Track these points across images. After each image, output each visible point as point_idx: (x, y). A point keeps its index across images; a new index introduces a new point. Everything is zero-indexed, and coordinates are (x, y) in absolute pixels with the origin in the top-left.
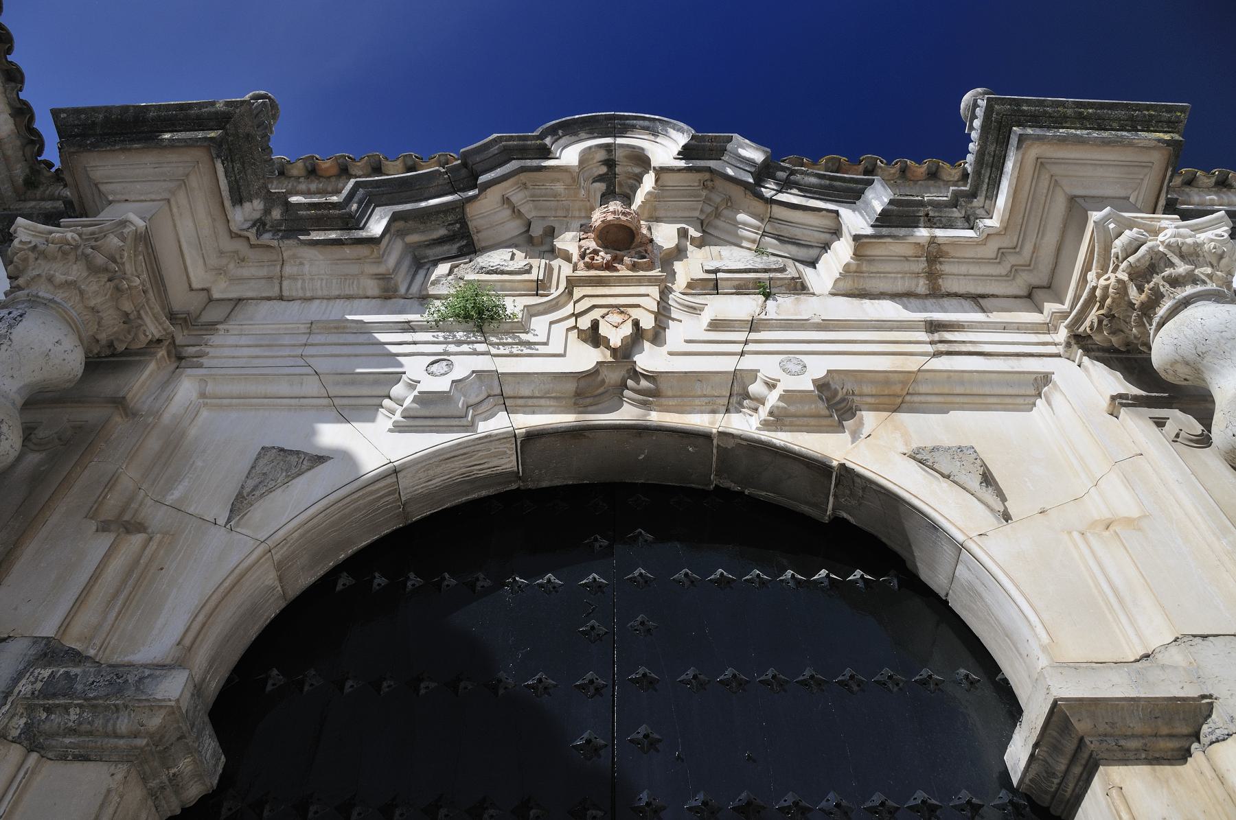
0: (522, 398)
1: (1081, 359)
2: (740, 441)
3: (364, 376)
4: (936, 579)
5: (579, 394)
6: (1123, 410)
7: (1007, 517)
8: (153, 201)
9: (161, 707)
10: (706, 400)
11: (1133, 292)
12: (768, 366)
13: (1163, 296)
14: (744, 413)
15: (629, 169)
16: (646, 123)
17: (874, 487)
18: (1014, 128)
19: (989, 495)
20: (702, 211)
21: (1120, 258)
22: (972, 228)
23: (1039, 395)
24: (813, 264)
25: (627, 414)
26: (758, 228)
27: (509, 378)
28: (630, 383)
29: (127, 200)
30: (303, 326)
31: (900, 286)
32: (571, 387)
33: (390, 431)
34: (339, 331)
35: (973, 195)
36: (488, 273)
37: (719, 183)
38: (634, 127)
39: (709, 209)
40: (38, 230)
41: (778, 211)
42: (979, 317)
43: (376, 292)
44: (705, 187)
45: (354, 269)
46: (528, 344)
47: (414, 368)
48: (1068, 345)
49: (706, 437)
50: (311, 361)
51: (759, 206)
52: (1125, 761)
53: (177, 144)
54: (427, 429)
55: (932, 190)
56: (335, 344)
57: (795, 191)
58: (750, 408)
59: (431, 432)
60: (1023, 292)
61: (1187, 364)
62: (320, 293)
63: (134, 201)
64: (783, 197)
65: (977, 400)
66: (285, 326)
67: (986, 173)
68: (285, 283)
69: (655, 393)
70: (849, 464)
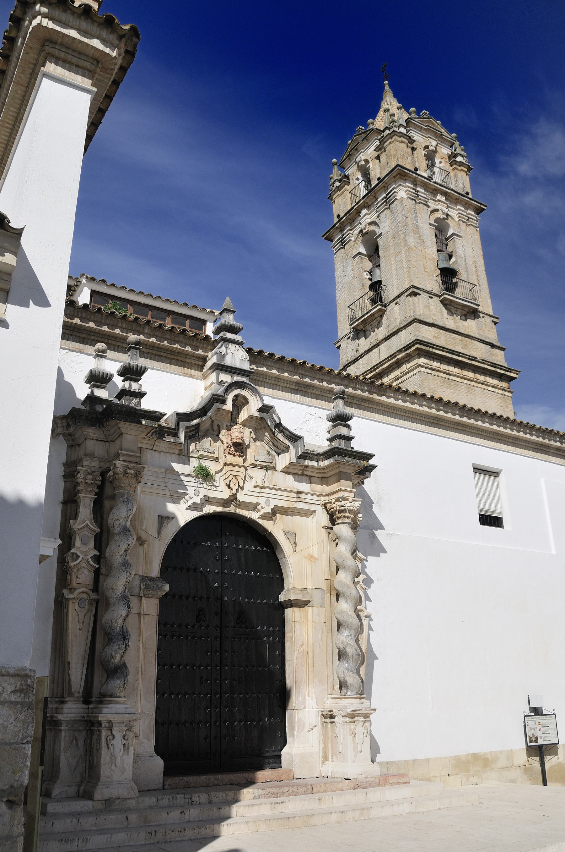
4: (279, 556)
7: (295, 551)
11: (337, 512)
12: (262, 501)
15: (242, 400)
16: (251, 388)
19: (294, 546)
20: (257, 426)
24: (278, 454)
31: (296, 472)
38: (247, 387)
46: (215, 486)
47: (191, 490)
50: (168, 485)
52: (296, 607)
67: (326, 455)
68: (155, 446)
70: (272, 532)
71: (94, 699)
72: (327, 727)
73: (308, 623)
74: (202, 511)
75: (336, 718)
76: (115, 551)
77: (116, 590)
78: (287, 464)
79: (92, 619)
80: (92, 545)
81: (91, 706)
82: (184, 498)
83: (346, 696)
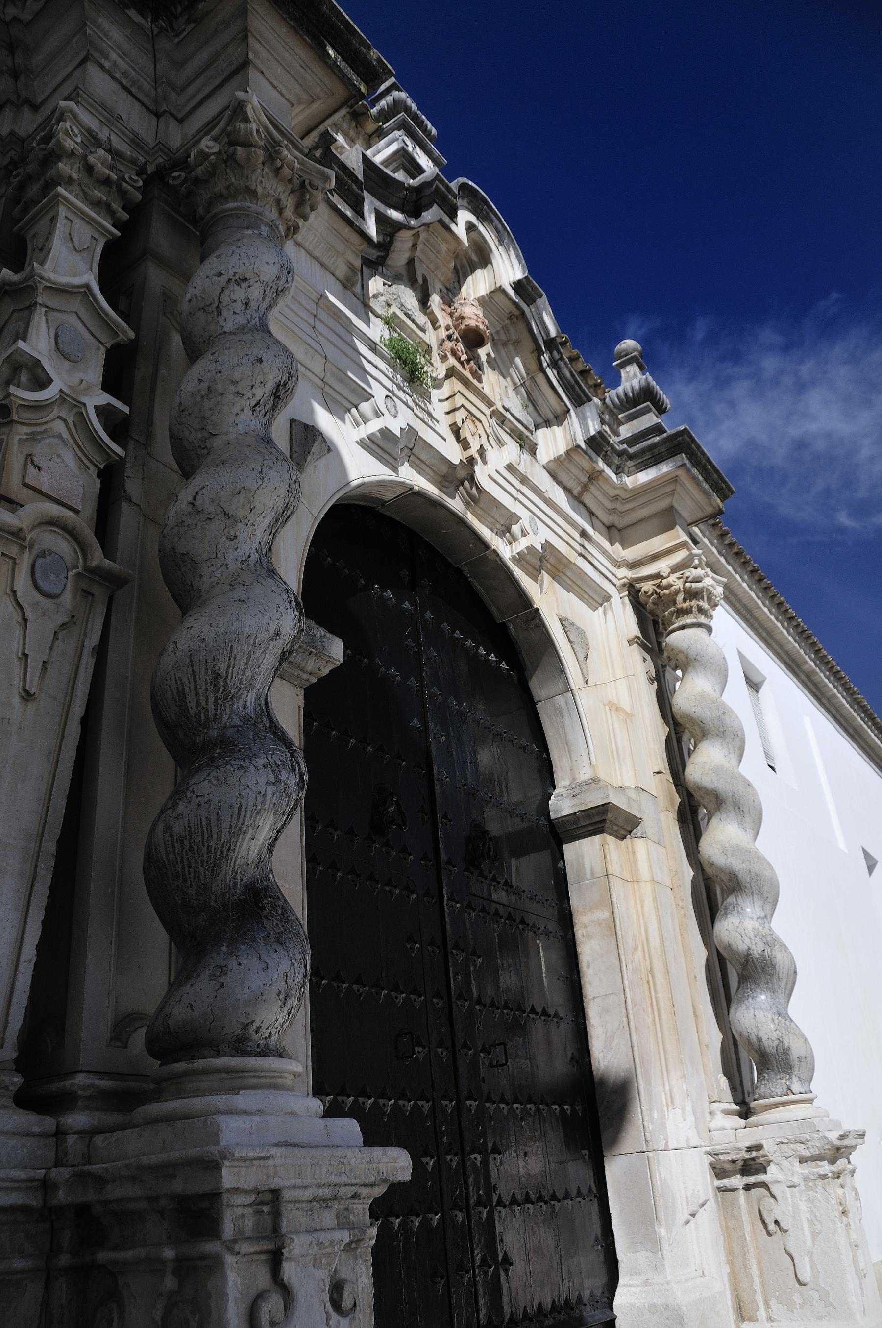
0: (419, 459)
1: (625, 596)
2: (498, 559)
3: (350, 380)
5: (444, 477)
6: (635, 645)
8: (282, 95)
9: (333, 663)
10: (494, 521)
11: (680, 598)
13: (692, 612)
14: (504, 541)
16: (500, 227)
17: (544, 630)
18: (683, 455)
21: (689, 580)
22: (616, 474)
23: (601, 605)
25: (456, 504)
26: (523, 378)
27: (421, 442)
28: (466, 483)
29: (262, 72)
30: (315, 294)
32: (444, 469)
33: (357, 442)
34: (335, 317)
35: (631, 457)
36: (406, 314)
37: (521, 326)
38: (492, 222)
39: (503, 337)
40: (260, 118)
41: (540, 378)
42: (606, 544)
43: (341, 276)
44: (510, 318)
45: (340, 246)
48: (624, 585)
49: (486, 546)
51: (534, 366)
53: (336, 71)
54: (376, 455)
55: (791, 646)
56: (330, 329)
57: (555, 372)
58: (508, 540)
59: (377, 458)
60: (607, 524)
61: (687, 658)
62: (307, 245)
63: (267, 79)
64: (548, 371)
65: (582, 592)
66: (304, 284)
67: (648, 455)
69: (475, 501)
70: (540, 610)
71: (82, 1079)
72: (735, 1203)
73: (642, 884)
74: (395, 469)
75: (772, 1169)
76: (237, 376)
77: (240, 527)
78: (562, 451)
79: (88, 663)
80: (94, 373)
81: (78, 1120)
82: (356, 407)
83: (791, 1097)
